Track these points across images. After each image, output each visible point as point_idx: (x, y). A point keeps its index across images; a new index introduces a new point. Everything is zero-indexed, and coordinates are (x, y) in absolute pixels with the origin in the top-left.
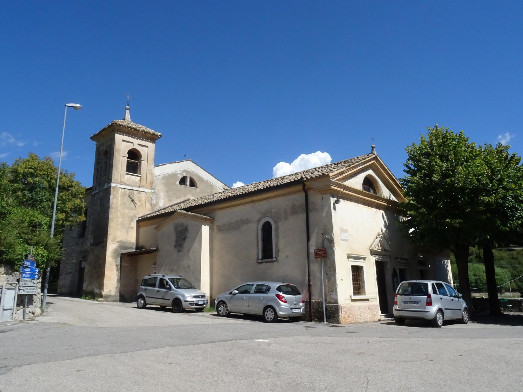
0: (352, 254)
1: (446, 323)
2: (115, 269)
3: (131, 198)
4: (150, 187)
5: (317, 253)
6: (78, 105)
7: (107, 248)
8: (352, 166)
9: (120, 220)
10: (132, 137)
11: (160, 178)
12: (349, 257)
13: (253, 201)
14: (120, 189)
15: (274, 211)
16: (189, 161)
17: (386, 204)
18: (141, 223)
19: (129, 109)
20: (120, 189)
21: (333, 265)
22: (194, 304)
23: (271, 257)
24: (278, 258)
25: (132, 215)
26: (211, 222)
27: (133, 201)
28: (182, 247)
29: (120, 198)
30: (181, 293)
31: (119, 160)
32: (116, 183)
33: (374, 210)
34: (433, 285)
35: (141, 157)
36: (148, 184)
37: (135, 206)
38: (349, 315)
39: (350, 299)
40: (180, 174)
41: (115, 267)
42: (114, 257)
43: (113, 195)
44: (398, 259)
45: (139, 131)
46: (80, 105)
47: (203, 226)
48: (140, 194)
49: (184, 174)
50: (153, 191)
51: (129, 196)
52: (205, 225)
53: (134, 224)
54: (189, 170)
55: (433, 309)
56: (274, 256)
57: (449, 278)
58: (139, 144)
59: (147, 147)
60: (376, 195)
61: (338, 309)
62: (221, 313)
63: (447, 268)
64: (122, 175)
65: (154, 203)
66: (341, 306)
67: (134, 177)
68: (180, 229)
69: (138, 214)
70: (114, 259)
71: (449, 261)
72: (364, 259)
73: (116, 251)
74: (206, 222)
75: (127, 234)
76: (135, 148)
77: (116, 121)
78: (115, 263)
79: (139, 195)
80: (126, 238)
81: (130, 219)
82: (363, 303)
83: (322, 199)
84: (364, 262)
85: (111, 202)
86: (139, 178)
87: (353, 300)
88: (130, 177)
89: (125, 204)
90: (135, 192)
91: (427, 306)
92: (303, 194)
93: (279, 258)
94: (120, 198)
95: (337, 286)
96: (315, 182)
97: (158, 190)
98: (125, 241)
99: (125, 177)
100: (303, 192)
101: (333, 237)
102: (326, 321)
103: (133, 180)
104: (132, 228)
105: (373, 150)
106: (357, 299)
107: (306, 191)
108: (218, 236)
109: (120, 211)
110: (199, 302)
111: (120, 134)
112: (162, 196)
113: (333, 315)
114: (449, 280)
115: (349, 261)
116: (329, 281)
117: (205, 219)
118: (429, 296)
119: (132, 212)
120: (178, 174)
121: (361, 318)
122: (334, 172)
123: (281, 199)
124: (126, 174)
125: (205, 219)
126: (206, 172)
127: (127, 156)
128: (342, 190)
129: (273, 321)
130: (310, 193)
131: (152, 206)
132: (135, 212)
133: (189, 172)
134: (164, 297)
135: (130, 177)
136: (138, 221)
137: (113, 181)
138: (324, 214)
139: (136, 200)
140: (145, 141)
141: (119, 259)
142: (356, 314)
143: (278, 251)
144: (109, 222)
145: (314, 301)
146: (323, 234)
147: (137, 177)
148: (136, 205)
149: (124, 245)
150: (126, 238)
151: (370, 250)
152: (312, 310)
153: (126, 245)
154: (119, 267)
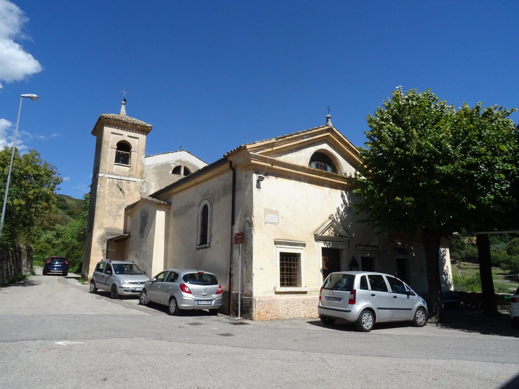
0: (283, 239)
1: (377, 326)
2: (101, 254)
3: (119, 187)
4: (140, 176)
5: (237, 237)
6: (35, 96)
7: (93, 234)
8: (287, 138)
9: (107, 208)
10: (121, 130)
11: (151, 168)
12: (276, 243)
13: (197, 184)
14: (108, 179)
15: (211, 192)
16: (184, 151)
17: (346, 183)
18: (129, 211)
19: (124, 104)
20: (108, 179)
21: (251, 251)
22: (129, 290)
23: (206, 243)
24: (211, 244)
25: (121, 203)
26: (167, 207)
27: (121, 190)
28: (143, 233)
29: (107, 188)
30: (118, 279)
31: (107, 152)
32: (104, 173)
33: (327, 190)
34: (363, 279)
35: (131, 148)
36: (138, 174)
37: (124, 195)
38: (267, 310)
39: (274, 291)
40: (173, 164)
41: (102, 252)
42: (100, 243)
43: (101, 184)
44: (359, 245)
45: (127, 123)
46: (37, 95)
47: (158, 212)
48: (129, 183)
49: (177, 164)
50: (143, 181)
51: (117, 185)
52: (160, 210)
53: (122, 212)
54: (183, 160)
55: (358, 307)
56: (208, 242)
57: (445, 268)
58: (128, 136)
59: (138, 138)
60: (327, 172)
61: (252, 303)
62: (142, 301)
63: (443, 257)
64: (111, 165)
65: (145, 191)
66: (255, 300)
67: (124, 167)
68: (463, 231)
69: (126, 202)
70: (100, 244)
71: (448, 250)
72: (304, 245)
73: (102, 238)
74: (161, 207)
75: (115, 222)
76: (125, 139)
77: (104, 115)
78: (101, 248)
79: (129, 184)
80: (114, 225)
81: (118, 207)
82: (296, 296)
83: (246, 177)
84: (302, 249)
85: (98, 191)
86: (129, 168)
87: (277, 293)
88: (119, 167)
89: (113, 193)
90: (124, 181)
91: (349, 304)
92: (231, 172)
93: (212, 244)
94: (107, 188)
95: (253, 276)
96: (236, 157)
97: (149, 179)
98: (113, 227)
99: (114, 168)
100: (231, 170)
101: (253, 219)
102: (241, 317)
103: (122, 170)
104: (120, 216)
105: (327, 121)
106: (281, 292)
107: (233, 169)
108: (172, 220)
109: (107, 200)
110: (136, 289)
111: (109, 127)
112: (153, 186)
113: (247, 310)
114: (446, 271)
115: (276, 247)
116: (247, 269)
117: (160, 204)
118: (354, 292)
119: (120, 200)
120: (171, 164)
121: (288, 313)
122: (255, 143)
123: (216, 179)
124: (115, 164)
125: (160, 204)
126: (202, 162)
127: (116, 148)
128: (270, 165)
129: (175, 314)
130: (238, 171)
131: (141, 194)
132: (124, 201)
133: (184, 162)
134: (106, 283)
135: (119, 167)
136: (126, 210)
137: (100, 171)
138: (247, 194)
139: (124, 189)
140: (136, 133)
141: (106, 245)
142: (280, 309)
143: (212, 235)
144: (96, 210)
145: (234, 292)
146: (245, 216)
147: (127, 167)
148: (124, 193)
149: (111, 231)
150: (114, 225)
151: (315, 235)
152: (231, 302)
153: (113, 232)
154: (105, 252)
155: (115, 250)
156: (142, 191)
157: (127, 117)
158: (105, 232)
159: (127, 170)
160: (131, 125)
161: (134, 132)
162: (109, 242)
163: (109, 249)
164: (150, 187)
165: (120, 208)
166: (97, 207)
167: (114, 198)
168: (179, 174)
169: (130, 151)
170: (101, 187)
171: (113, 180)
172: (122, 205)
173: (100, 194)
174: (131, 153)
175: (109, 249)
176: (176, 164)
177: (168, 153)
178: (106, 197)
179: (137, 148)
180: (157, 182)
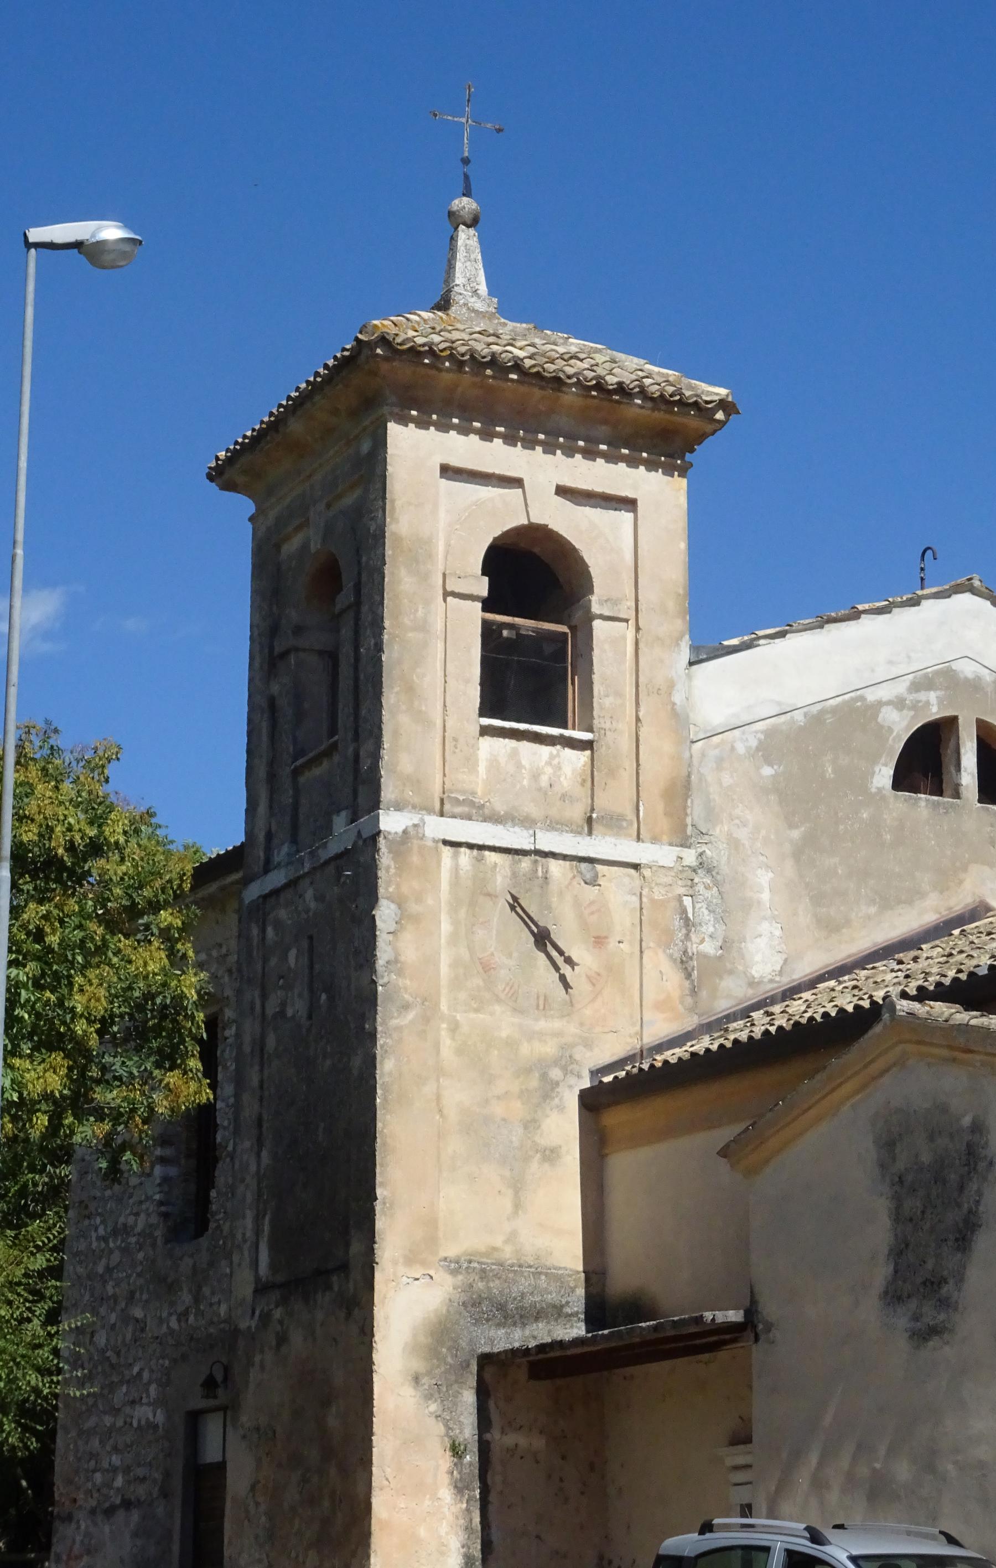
3: (527, 919)
6: (111, 232)
7: (379, 1313)
10: (510, 440)
11: (741, 749)
18: (616, 1118)
19: (473, 222)
20: (447, 851)
25: (549, 1049)
27: (542, 939)
29: (446, 927)
31: (423, 627)
37: (563, 979)
40: (899, 703)
41: (445, 1461)
43: (400, 903)
45: (557, 382)
46: (127, 225)
48: (593, 882)
50: (690, 857)
51: (515, 903)
54: (967, 669)
59: (629, 504)
65: (709, 948)
67: (545, 751)
69: (588, 1044)
70: (428, 1397)
75: (518, 1206)
76: (537, 519)
77: (384, 325)
78: (440, 1429)
79: (591, 893)
81: (534, 1082)
85: (383, 953)
88: (515, 753)
89: (487, 968)
90: (555, 867)
94: (446, 927)
97: (734, 844)
98: (508, 1254)
104: (551, 1155)
109: (454, 1028)
111: (423, 424)
112: (766, 896)
120: (880, 704)
124: (486, 731)
127: (485, 593)
132: (571, 1029)
137: (388, 792)
140: (611, 458)
141: (469, 1397)
147: (568, 752)
148: (566, 970)
149: (495, 1285)
150: (512, 1237)
154: (471, 1458)
155: (539, 1443)
156: (693, 948)
157: (508, 328)
158: (460, 1297)
159: (567, 770)
160: (579, 402)
161: (476, 432)
162: (488, 1376)
163: (495, 1435)
164: (747, 906)
165: (549, 1089)
166: (386, 1090)
167: (498, 1008)
168: (938, 791)
169: (578, 616)
170: (404, 918)
171: (480, 860)
172: (556, 1062)
173: (401, 982)
174: (583, 632)
175: (495, 1435)
176: (915, 707)
177: (855, 615)
178: (444, 1007)
179: (629, 590)
180: (789, 868)
